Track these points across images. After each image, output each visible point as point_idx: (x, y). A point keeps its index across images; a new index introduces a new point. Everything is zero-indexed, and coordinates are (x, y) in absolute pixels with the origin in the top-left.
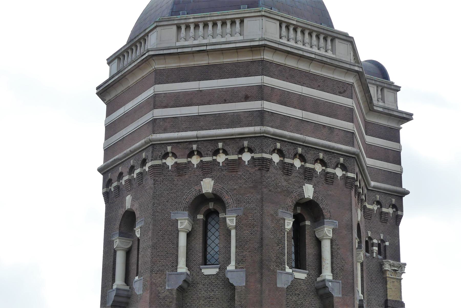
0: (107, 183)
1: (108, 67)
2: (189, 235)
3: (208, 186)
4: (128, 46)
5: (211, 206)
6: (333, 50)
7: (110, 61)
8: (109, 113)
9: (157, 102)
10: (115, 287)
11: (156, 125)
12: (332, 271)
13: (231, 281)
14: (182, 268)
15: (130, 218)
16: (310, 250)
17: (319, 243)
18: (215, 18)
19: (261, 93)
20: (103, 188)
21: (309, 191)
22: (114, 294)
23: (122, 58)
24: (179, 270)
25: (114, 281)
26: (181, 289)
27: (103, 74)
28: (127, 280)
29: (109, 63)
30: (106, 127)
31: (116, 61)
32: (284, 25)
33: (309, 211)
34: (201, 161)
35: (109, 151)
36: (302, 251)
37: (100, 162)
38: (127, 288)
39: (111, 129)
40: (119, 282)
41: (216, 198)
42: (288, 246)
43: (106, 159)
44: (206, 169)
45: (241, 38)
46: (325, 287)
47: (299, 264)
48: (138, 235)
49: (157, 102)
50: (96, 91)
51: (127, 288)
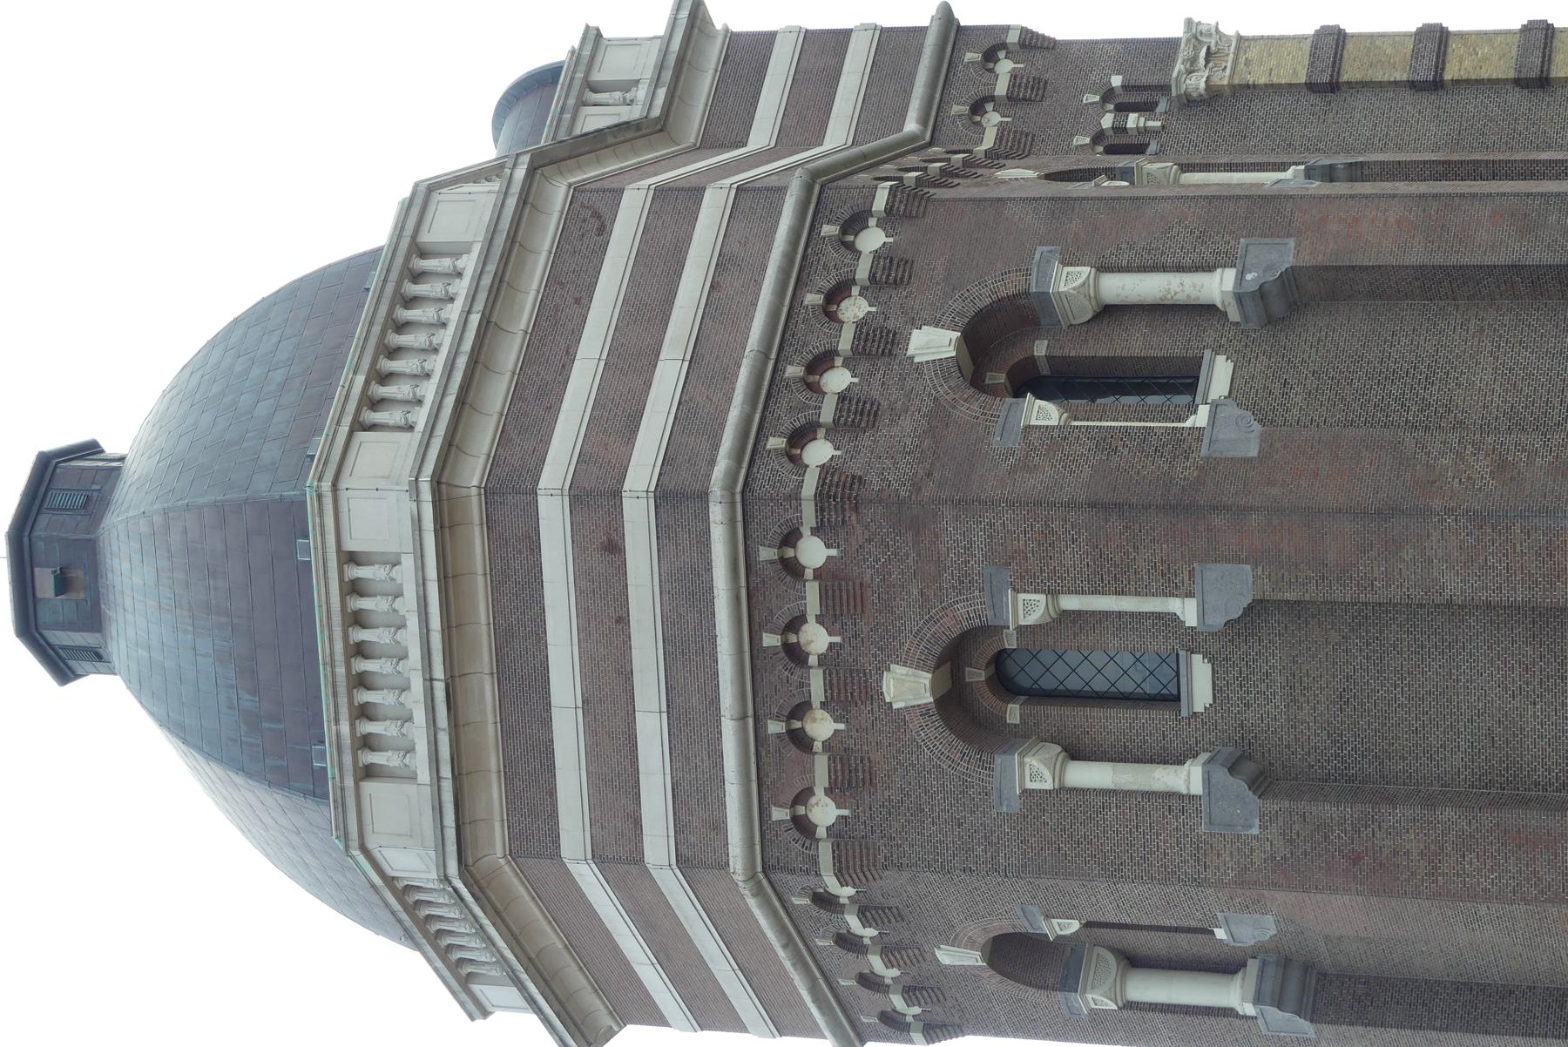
2: (1075, 753)
3: (907, 687)
5: (977, 675)
6: (457, 251)
7: (479, 1010)
9: (618, 851)
11: (697, 857)
14: (1187, 778)
16: (1134, 343)
17: (1110, 313)
18: (339, 647)
19: (596, 498)
21: (933, 343)
22: (1273, 1012)
23: (435, 927)
24: (1197, 788)
25: (1227, 1012)
26: (1261, 784)
28: (1225, 966)
29: (485, 1013)
34: (824, 705)
36: (1126, 369)
38: (1253, 966)
41: (951, 659)
43: (812, 1031)
45: (408, 562)
46: (1261, 293)
47: (1182, 381)
49: (618, 851)
51: (1253, 966)
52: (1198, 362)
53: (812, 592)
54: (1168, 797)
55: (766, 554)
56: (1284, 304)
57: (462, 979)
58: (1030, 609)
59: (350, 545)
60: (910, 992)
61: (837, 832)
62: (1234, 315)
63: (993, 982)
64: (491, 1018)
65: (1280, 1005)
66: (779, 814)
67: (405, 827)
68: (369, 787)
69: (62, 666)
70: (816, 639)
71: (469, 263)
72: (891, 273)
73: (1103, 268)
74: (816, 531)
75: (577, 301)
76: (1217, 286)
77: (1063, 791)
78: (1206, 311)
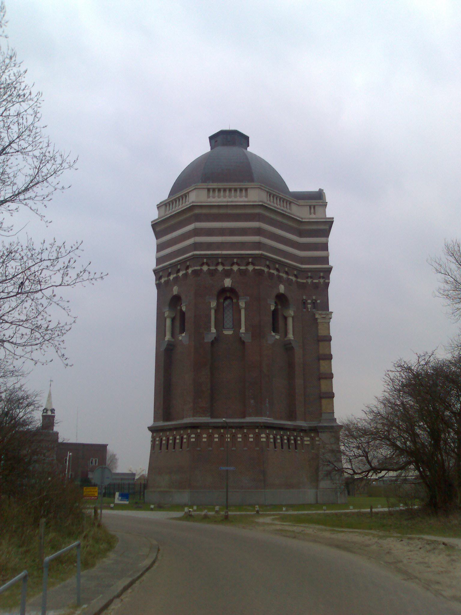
2: (216, 311)
3: (228, 282)
5: (228, 294)
6: (290, 209)
7: (159, 207)
9: (197, 232)
11: (196, 246)
12: (293, 335)
13: (243, 339)
14: (213, 330)
17: (285, 318)
18: (231, 187)
19: (258, 232)
20: (156, 281)
21: (282, 289)
24: (212, 331)
25: (165, 336)
26: (212, 343)
27: (155, 215)
28: (173, 335)
29: (158, 208)
30: (157, 246)
32: (270, 194)
33: (281, 299)
34: (239, 269)
35: (159, 261)
36: (277, 322)
38: (173, 340)
39: (160, 248)
40: (168, 337)
41: (232, 290)
42: (269, 319)
44: (228, 274)
45: (246, 199)
46: (290, 344)
47: (275, 329)
48: (184, 309)
49: (197, 232)
50: (151, 224)
51: (173, 340)
52: (278, 333)
53: (228, 268)
54: (210, 327)
55: (220, 260)
56: (288, 348)
58: (242, 304)
59: (249, 190)
61: (247, 270)
62: (286, 339)
63: (170, 297)
64: (156, 209)
65: (168, 345)
66: (250, 260)
67: (196, 197)
68: (206, 190)
69: (212, 138)
70: (235, 268)
71: (289, 211)
72: (289, 282)
73: (293, 317)
74: (224, 269)
75: (176, 300)
76: (291, 336)
77: (211, 309)
78: (286, 333)
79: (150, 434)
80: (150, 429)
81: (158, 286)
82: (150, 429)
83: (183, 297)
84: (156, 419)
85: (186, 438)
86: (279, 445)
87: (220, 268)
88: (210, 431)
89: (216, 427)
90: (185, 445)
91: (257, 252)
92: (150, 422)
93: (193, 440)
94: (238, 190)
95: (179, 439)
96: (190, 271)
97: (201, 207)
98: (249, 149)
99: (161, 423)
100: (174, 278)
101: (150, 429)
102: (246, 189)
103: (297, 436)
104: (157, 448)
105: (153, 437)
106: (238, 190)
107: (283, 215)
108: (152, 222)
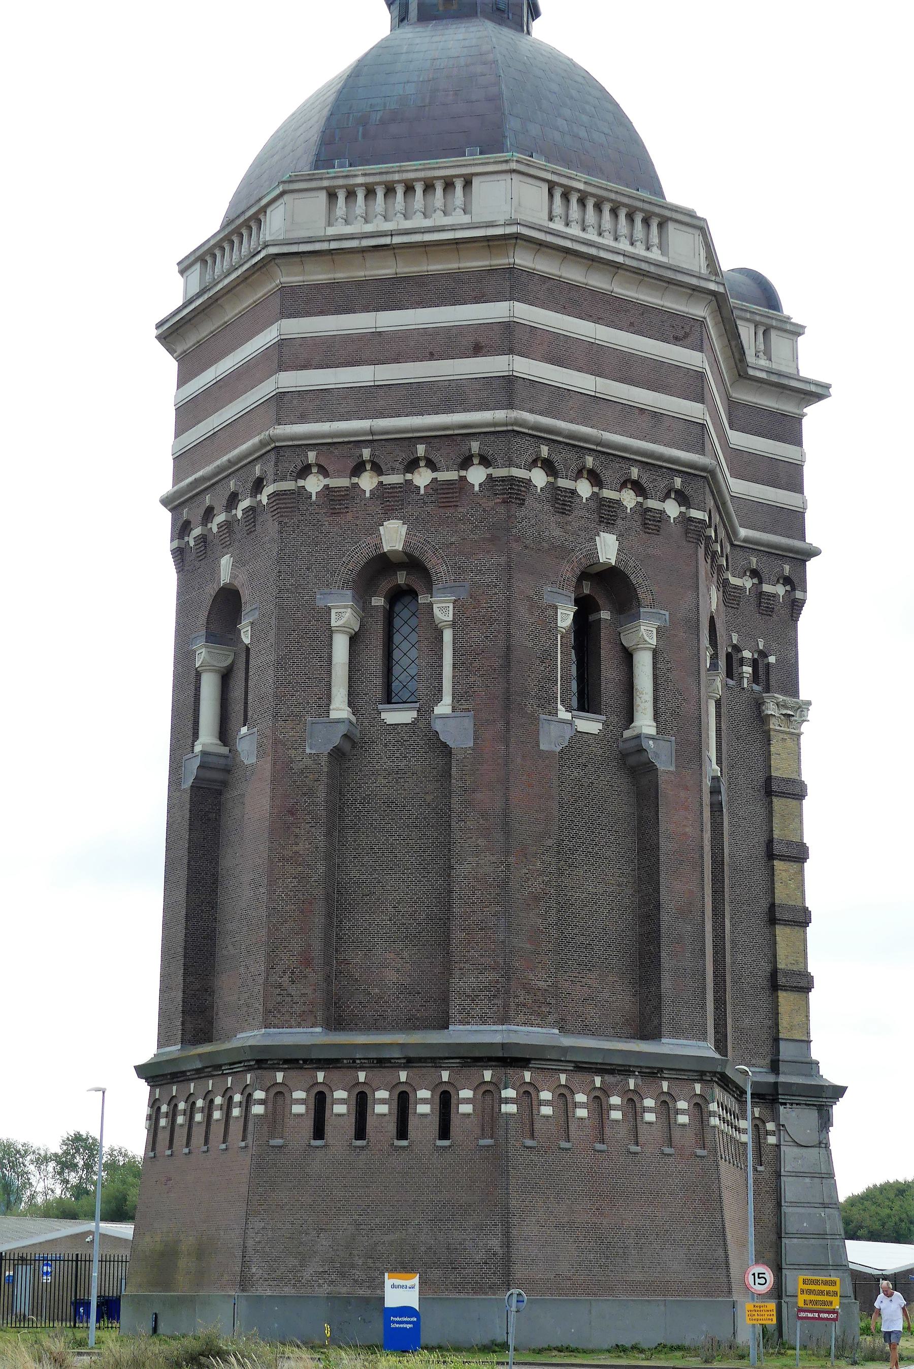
0: (181, 529)
1: (180, 281)
2: (354, 640)
3: (393, 536)
4: (222, 235)
5: (401, 578)
6: (663, 246)
7: (184, 268)
8: (183, 379)
9: (285, 356)
10: (198, 748)
11: (283, 405)
12: (656, 718)
14: (340, 709)
15: (228, 604)
16: (609, 671)
17: (628, 657)
18: (411, 175)
19: (508, 338)
20: (172, 540)
21: (607, 548)
22: (197, 762)
24: (334, 715)
25: (196, 735)
26: (337, 754)
27: (171, 294)
28: (224, 733)
29: (182, 272)
31: (198, 266)
35: (183, 461)
36: (593, 673)
37: (166, 485)
40: (207, 738)
41: (411, 562)
42: (563, 663)
43: (177, 478)
44: (391, 501)
46: (641, 750)
47: (587, 702)
49: (285, 356)
51: (224, 750)
56: (635, 766)
57: (203, 257)
58: (443, 610)
60: (203, 539)
62: (627, 734)
63: (211, 590)
64: (179, 275)
67: (297, 220)
68: (323, 196)
70: (422, 478)
71: (655, 255)
72: (651, 521)
74: (489, 476)
76: (645, 722)
79: (143, 1089)
80: (143, 1071)
81: (179, 554)
82: (150, 1073)
83: (245, 595)
84: (163, 1040)
85: (221, 1107)
86: (217, 1131)
87: (367, 482)
88: (563, 1078)
89: (584, 1067)
90: (236, 1129)
91: (500, 415)
92: (147, 1048)
93: (258, 1109)
94: (419, 188)
95: (221, 1107)
96: (264, 498)
97: (540, 246)
98: (539, 29)
99: (174, 1049)
100: (220, 526)
101: (143, 1071)
102: (468, 183)
103: (606, 1091)
104: (163, 1137)
105: (154, 1104)
106: (419, 188)
107: (641, 274)
108: (158, 326)
